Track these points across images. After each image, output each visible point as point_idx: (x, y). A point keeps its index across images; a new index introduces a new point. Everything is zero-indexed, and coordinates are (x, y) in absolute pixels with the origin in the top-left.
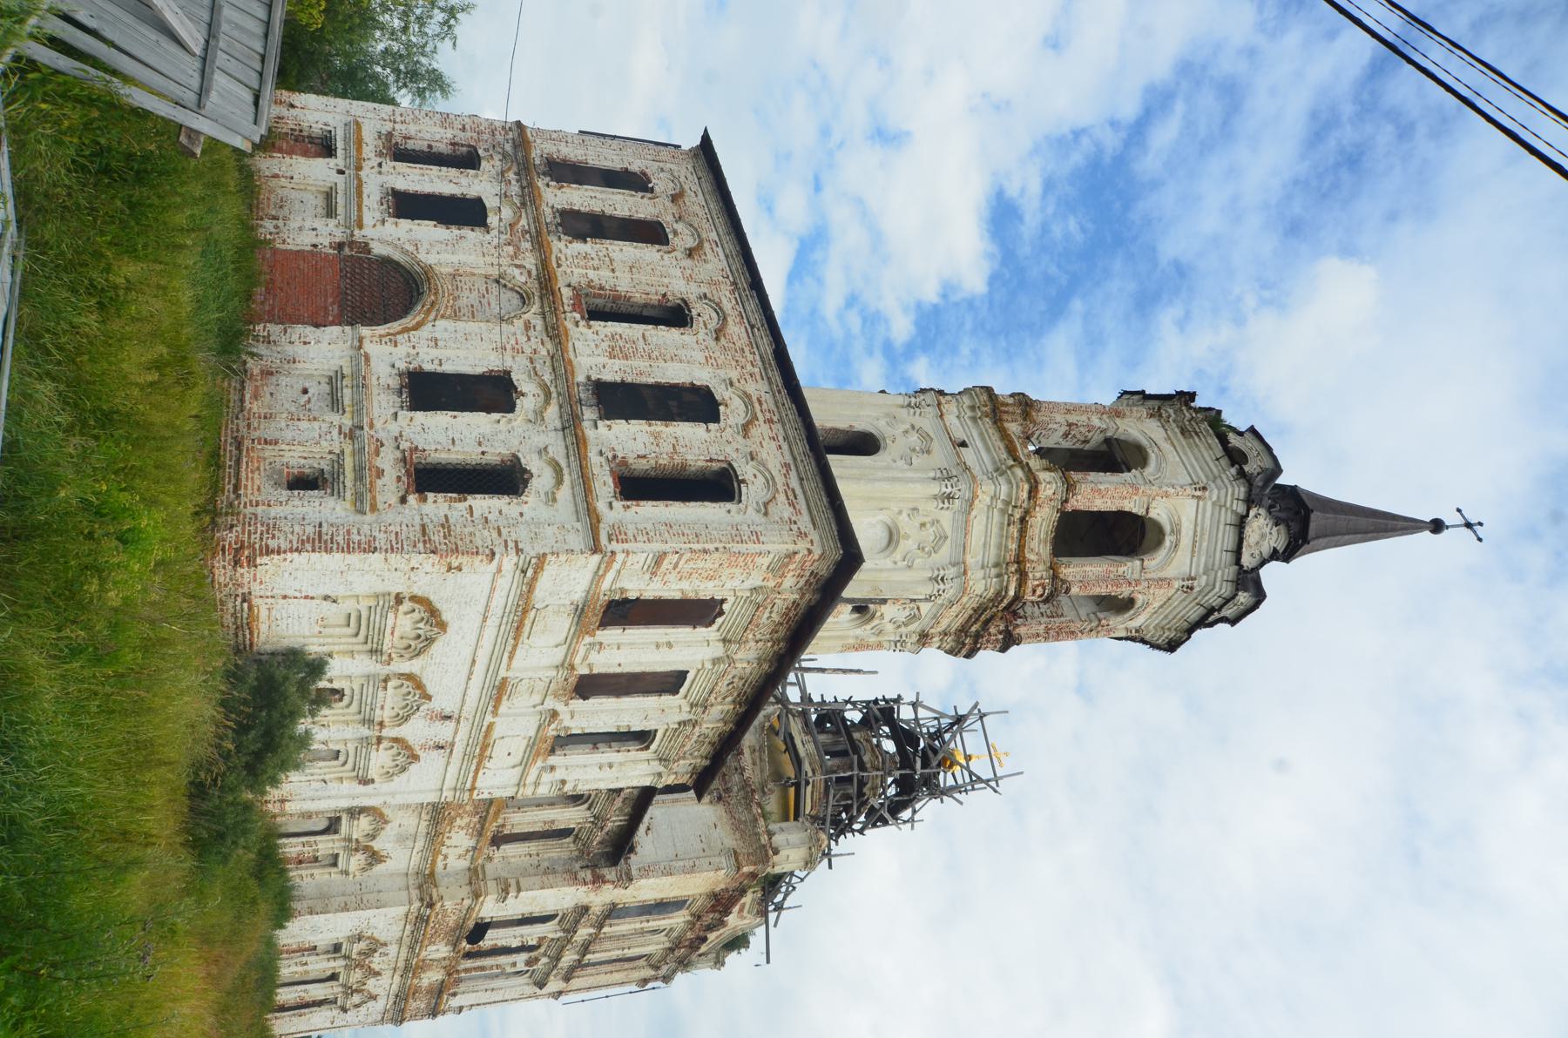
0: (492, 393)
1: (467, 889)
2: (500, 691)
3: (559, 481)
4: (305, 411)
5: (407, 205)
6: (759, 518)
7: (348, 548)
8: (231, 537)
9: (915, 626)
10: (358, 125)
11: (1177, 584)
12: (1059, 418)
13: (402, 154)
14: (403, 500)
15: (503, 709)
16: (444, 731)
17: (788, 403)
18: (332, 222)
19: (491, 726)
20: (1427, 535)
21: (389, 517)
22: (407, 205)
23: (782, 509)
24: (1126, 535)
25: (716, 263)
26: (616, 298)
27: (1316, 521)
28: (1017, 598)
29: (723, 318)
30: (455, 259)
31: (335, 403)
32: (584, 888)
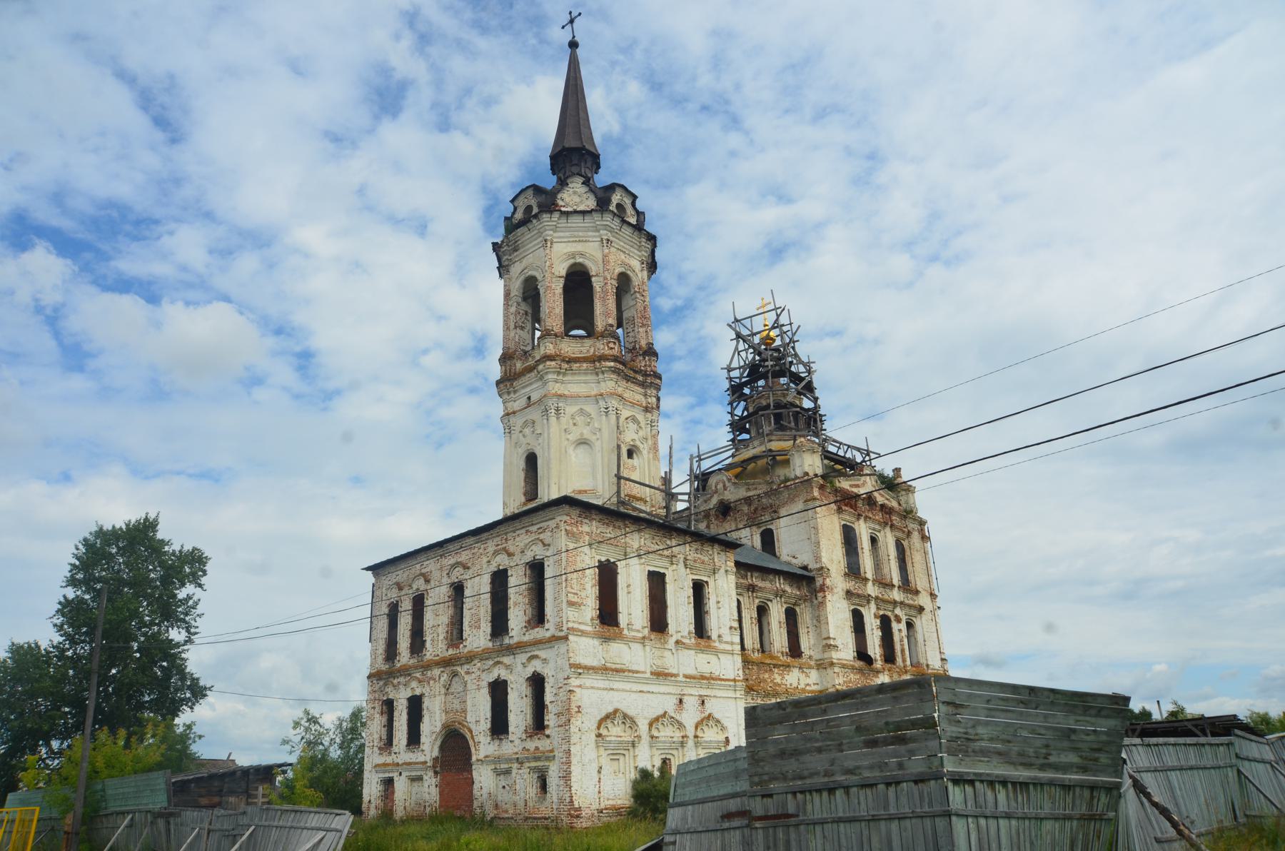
0: (499, 691)
1: (829, 671)
2: (661, 675)
3: (536, 657)
4: (511, 788)
5: (414, 738)
7: (569, 763)
9: (640, 417)
10: (377, 766)
12: (512, 334)
13: (389, 742)
14: (548, 736)
15: (674, 671)
17: (497, 530)
20: (580, 52)
21: (555, 743)
22: (414, 738)
23: (546, 536)
24: (578, 283)
25: (430, 565)
27: (571, 143)
28: (616, 359)
31: (507, 772)
32: (829, 597)
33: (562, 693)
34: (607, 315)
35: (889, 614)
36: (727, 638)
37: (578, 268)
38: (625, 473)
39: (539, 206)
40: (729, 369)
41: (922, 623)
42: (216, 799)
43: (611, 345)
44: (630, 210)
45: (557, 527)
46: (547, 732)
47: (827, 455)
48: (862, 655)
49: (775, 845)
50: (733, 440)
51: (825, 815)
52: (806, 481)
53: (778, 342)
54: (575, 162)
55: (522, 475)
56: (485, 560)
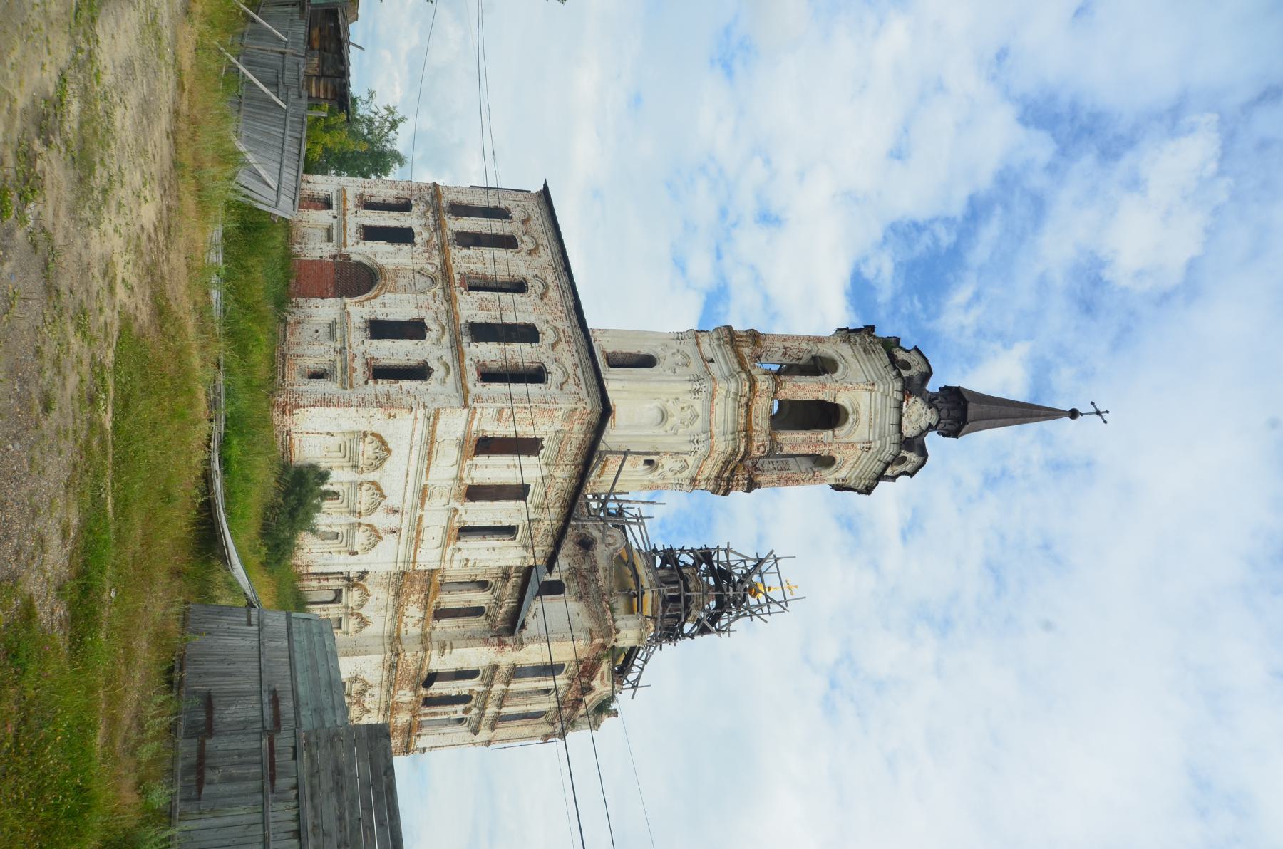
0: (415, 329)
1: (419, 647)
3: (448, 373)
5: (371, 233)
6: (558, 392)
7: (338, 405)
8: (281, 400)
9: (686, 474)
11: (859, 446)
12: (779, 344)
13: (369, 205)
14: (366, 383)
15: (426, 507)
16: (394, 521)
17: (580, 332)
18: (330, 244)
19: (421, 517)
22: (371, 233)
23: (571, 386)
24: (827, 416)
25: (546, 257)
26: (486, 279)
27: (972, 409)
28: (747, 453)
29: (546, 287)
30: (396, 261)
31: (332, 336)
32: (493, 649)
33: (410, 400)
34: (793, 445)
35: (473, 702)
36: (458, 556)
37: (842, 416)
38: (629, 458)
39: (910, 378)
40: (727, 551)
41: (462, 732)
42: (316, 45)
43: (762, 449)
44: (898, 469)
45: (580, 399)
46: (371, 382)
47: (632, 653)
48: (432, 678)
49: (243, 763)
50: (655, 550)
51: (271, 826)
52: (609, 631)
53: (752, 601)
54: (952, 413)
55: (634, 351)
56: (550, 318)
